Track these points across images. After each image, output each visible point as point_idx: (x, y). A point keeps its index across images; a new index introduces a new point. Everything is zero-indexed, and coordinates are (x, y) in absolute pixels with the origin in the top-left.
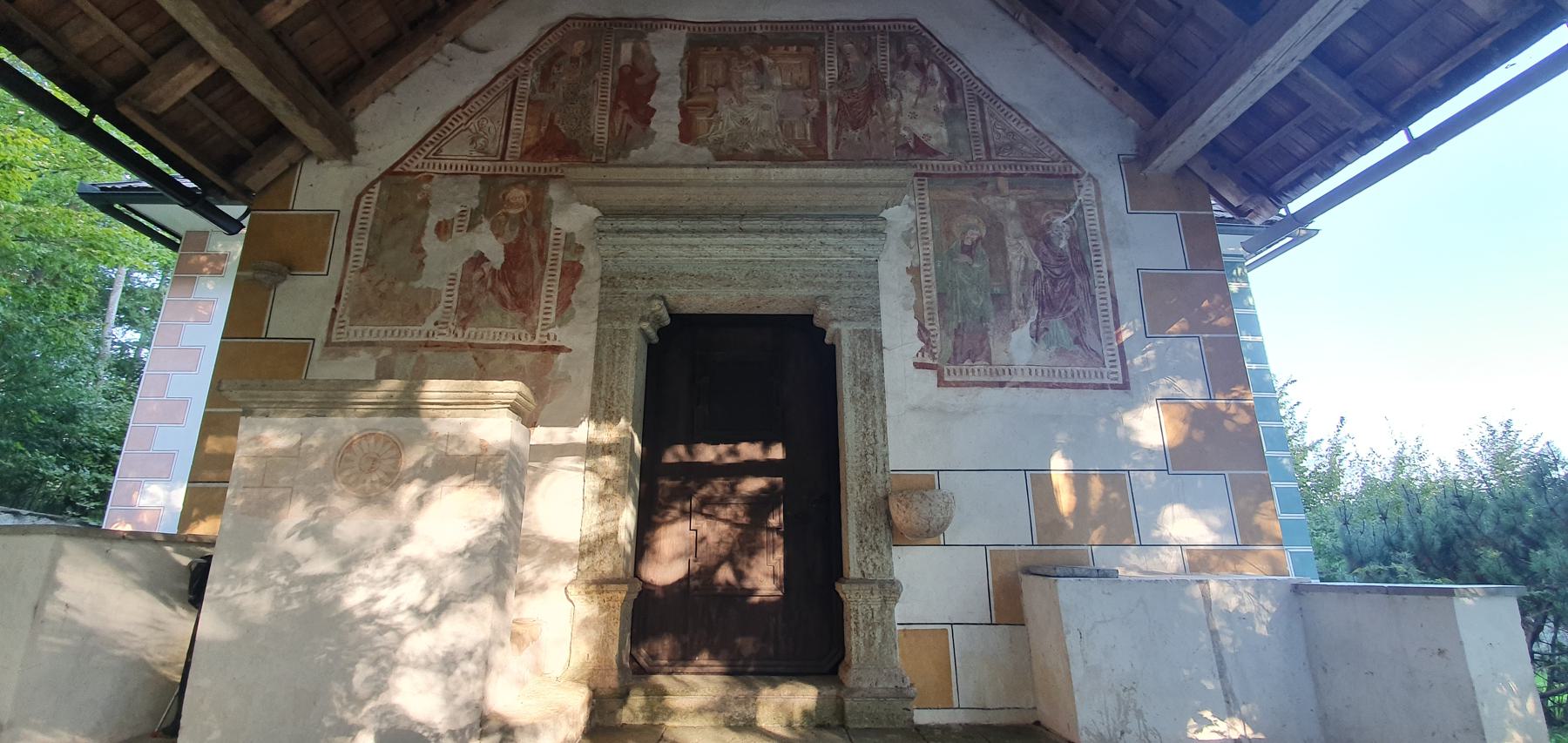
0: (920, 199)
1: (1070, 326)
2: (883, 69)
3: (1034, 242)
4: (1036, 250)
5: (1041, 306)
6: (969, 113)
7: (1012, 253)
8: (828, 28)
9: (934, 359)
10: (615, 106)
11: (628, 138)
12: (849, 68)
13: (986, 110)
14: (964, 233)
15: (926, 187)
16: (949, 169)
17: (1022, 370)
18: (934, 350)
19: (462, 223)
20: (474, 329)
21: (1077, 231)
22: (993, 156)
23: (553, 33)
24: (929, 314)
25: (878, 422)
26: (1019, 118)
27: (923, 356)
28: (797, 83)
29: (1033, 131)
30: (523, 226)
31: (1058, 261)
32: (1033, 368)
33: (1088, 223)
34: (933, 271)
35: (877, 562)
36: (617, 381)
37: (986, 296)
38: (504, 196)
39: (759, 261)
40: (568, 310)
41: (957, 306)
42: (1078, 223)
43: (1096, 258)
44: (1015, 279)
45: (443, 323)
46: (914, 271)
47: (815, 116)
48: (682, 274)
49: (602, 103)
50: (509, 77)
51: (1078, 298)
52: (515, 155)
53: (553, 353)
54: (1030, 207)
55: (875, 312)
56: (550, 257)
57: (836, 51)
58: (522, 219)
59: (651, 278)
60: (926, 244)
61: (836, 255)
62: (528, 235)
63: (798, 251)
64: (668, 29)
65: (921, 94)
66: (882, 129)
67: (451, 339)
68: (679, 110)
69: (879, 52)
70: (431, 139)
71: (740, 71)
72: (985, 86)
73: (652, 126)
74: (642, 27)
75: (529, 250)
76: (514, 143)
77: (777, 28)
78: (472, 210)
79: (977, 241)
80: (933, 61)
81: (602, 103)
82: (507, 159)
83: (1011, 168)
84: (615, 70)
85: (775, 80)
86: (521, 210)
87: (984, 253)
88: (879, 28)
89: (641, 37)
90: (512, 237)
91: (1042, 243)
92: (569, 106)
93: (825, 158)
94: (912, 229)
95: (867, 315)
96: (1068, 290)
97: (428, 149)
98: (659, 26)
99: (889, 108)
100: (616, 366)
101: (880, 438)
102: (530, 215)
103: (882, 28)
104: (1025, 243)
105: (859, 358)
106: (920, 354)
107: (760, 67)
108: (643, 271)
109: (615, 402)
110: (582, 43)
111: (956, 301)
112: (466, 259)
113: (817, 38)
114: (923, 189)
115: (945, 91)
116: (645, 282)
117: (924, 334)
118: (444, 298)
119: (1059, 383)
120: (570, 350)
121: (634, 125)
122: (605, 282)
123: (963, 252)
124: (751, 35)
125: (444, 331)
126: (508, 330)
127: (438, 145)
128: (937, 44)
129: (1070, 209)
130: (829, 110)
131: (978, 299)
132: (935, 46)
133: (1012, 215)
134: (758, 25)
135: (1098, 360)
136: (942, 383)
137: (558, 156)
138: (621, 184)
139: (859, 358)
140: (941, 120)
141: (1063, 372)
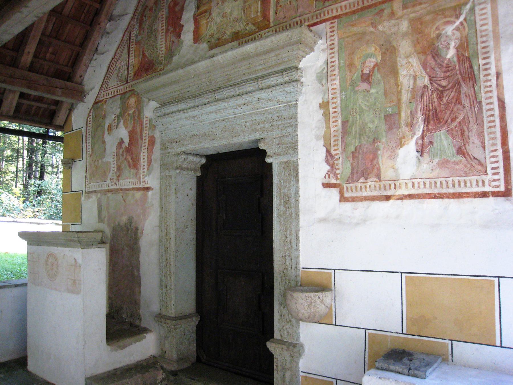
1: (454, 138)
3: (423, 58)
4: (425, 66)
5: (427, 121)
7: (403, 73)
9: (337, 179)
14: (364, 63)
15: (335, 29)
17: (406, 183)
18: (338, 172)
21: (467, 37)
25: (293, 232)
27: (329, 177)
30: (134, 120)
31: (445, 72)
32: (416, 182)
33: (479, 23)
35: (289, 330)
39: (228, 119)
41: (356, 131)
42: (468, 26)
43: (484, 61)
44: (405, 97)
46: (324, 106)
48: (193, 136)
51: (464, 107)
53: (147, 191)
54: (421, 23)
61: (269, 106)
63: (245, 108)
79: (374, 68)
90: (130, 129)
91: (430, 57)
94: (324, 69)
96: (454, 101)
101: (294, 244)
102: (137, 113)
104: (415, 62)
105: (282, 184)
106: (327, 176)
111: (356, 127)
117: (330, 159)
119: (440, 194)
122: (162, 147)
129: (460, 14)
131: (373, 122)
135: (480, 168)
136: (343, 199)
138: (164, 86)
139: (282, 184)
141: (444, 183)
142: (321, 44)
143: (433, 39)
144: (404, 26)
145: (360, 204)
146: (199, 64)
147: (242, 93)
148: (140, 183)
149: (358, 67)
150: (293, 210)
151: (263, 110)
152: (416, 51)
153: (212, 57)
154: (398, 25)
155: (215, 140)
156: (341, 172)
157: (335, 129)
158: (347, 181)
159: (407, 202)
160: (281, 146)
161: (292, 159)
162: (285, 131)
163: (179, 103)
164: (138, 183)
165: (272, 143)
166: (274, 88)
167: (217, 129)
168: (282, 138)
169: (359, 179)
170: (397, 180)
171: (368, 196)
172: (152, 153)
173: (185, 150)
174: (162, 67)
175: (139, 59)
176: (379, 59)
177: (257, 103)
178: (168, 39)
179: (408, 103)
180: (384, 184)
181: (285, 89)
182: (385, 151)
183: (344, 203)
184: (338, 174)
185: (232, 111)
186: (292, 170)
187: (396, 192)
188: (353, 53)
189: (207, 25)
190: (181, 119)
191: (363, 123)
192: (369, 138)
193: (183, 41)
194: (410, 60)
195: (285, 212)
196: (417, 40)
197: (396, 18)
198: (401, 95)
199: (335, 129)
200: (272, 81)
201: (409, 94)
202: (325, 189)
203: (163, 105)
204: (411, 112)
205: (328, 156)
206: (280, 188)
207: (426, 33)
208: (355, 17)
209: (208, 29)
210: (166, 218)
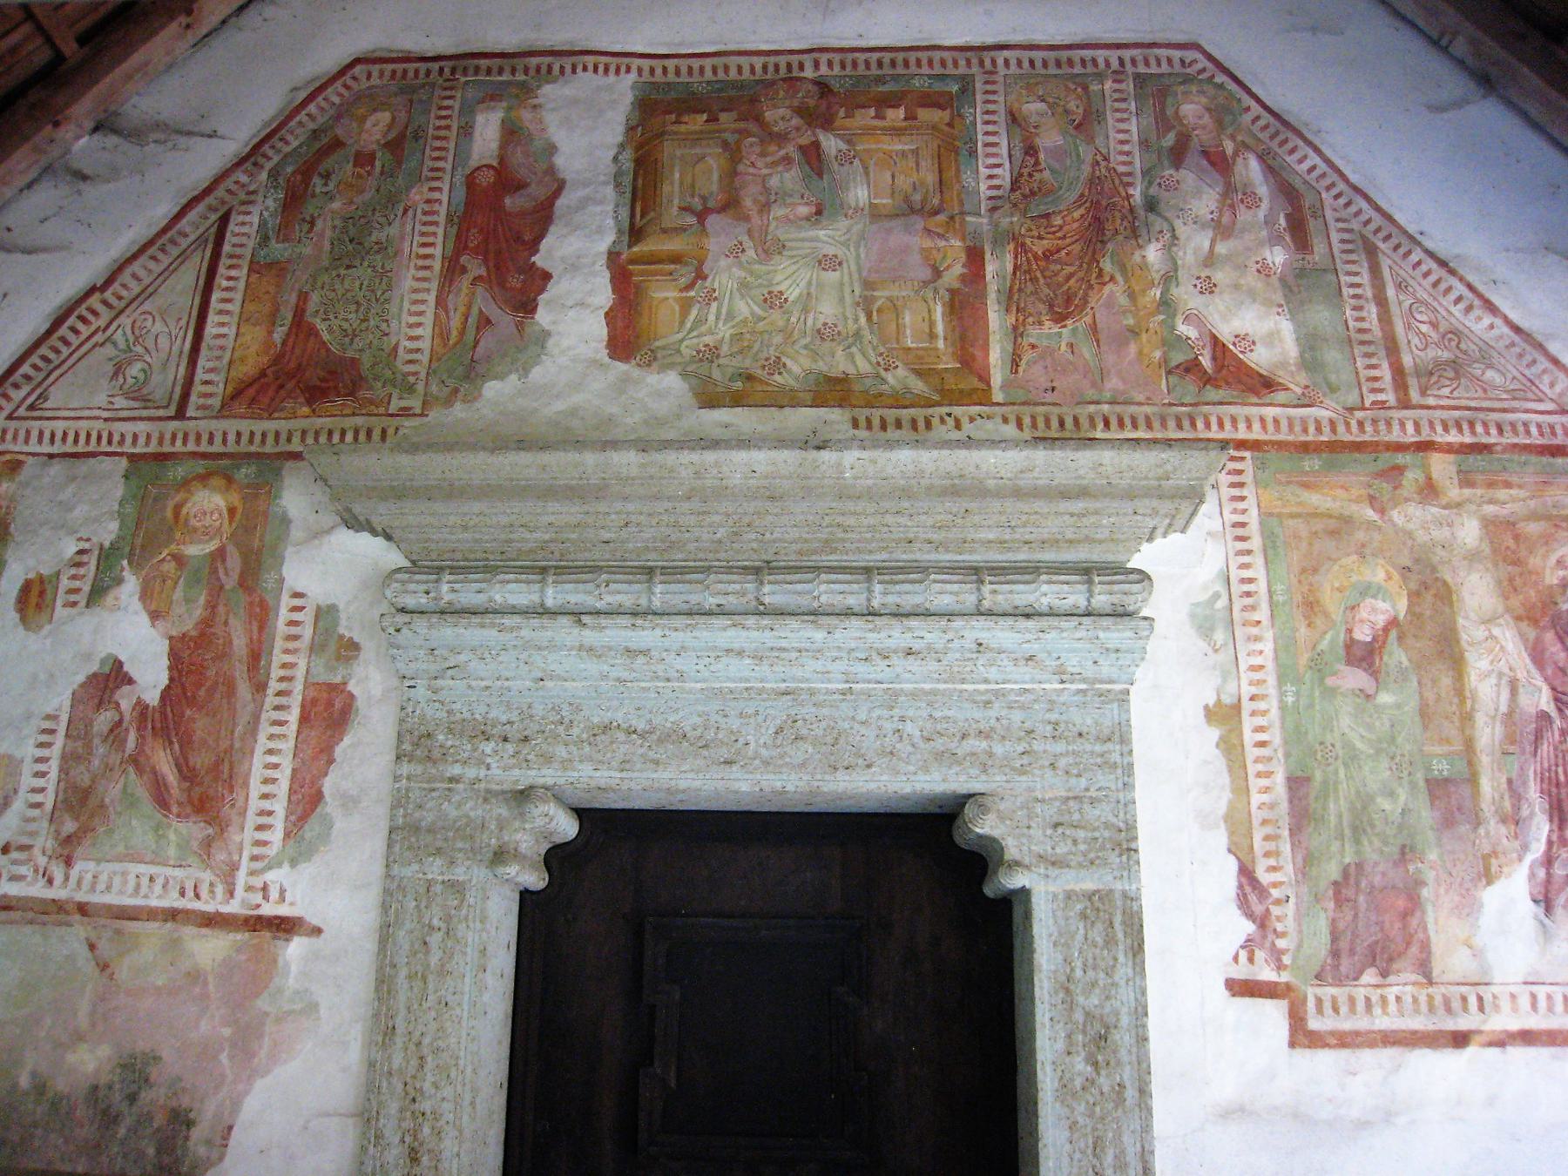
0: (1235, 511)
2: (1124, 163)
3: (1532, 634)
6: (1344, 279)
7: (1478, 664)
8: (981, 63)
9: (1280, 967)
10: (452, 269)
11: (480, 350)
12: (1037, 163)
13: (1386, 273)
15: (1248, 478)
16: (1305, 431)
17: (1513, 996)
19: (77, 584)
20: (91, 865)
22: (1414, 395)
23: (320, 99)
24: (1267, 838)
26: (1470, 295)
28: (907, 199)
29: (1506, 330)
30: (217, 590)
32: (1541, 992)
34: (1274, 713)
36: (433, 1026)
37: (1413, 786)
38: (178, 508)
39: (812, 692)
40: (314, 820)
41: (1340, 816)
44: (1487, 734)
45: (22, 848)
46: (1224, 715)
47: (956, 285)
48: (606, 728)
49: (421, 263)
50: (211, 209)
52: (210, 401)
53: (275, 938)
54: (1516, 537)
55: (1124, 843)
56: (276, 673)
57: (1001, 117)
58: (214, 571)
59: (526, 739)
60: (1257, 639)
61: (1020, 678)
62: (227, 614)
63: (913, 664)
64: (590, 73)
65: (1222, 230)
66: (1130, 321)
67: (38, 890)
68: (607, 275)
69: (1110, 122)
70: (26, 368)
71: (765, 171)
72: (1378, 209)
73: (543, 316)
74: (526, 71)
75: (224, 655)
76: (212, 370)
77: (855, 64)
78: (101, 547)
79: (1386, 630)
80: (1247, 147)
81: (421, 263)
82: (190, 412)
83: (1460, 430)
84: (459, 179)
85: (851, 195)
86: (212, 546)
87: (1406, 663)
88: (1108, 64)
89: (525, 92)
90: (187, 618)
92: (343, 272)
93: (982, 396)
94: (1217, 596)
95: (1103, 848)
97: (17, 395)
98: (568, 69)
99: (1144, 266)
100: (431, 986)
102: (234, 561)
103: (1115, 65)
104: (1510, 642)
105: (1079, 973)
106: (1243, 955)
107: (813, 157)
108: (504, 718)
109: (427, 1086)
110: (384, 117)
111: (1337, 800)
112: (81, 678)
113: (955, 88)
114: (1241, 485)
115: (1282, 221)
116: (510, 748)
117: (1253, 898)
118: (27, 781)
120: (317, 931)
121: (493, 311)
122: (407, 747)
123: (1352, 660)
124: (791, 81)
125: (23, 870)
126: (169, 871)
127: (40, 383)
128: (1253, 103)
130: (990, 268)
131: (1392, 794)
132: (1248, 109)
133: (1472, 557)
134: (808, 60)
136: (1301, 1036)
137: (309, 403)
140: (1279, 297)
142: (1209, 517)
143: (1551, 587)
144: (1469, 532)
145: (1367, 1056)
146: (741, 456)
147: (894, 609)
148: (231, 894)
149: (1334, 617)
150: (1127, 1075)
151: (983, 687)
152: (1508, 610)
153: (819, 448)
154: (1450, 525)
155: (735, 768)
156: (1292, 946)
157: (1265, 798)
158: (1318, 977)
159: (1517, 1053)
160: (1068, 832)
161: (1118, 886)
162: (1083, 782)
163: (550, 579)
164: (212, 892)
165: (1029, 817)
166: (1054, 621)
167: (752, 720)
168: (1071, 803)
169: (1361, 972)
170: (1486, 984)
171: (1393, 1031)
172: (331, 761)
173: (562, 781)
174: (415, 403)
175: (270, 333)
176: (1402, 605)
177: (969, 659)
178: (458, 301)
179: (1498, 754)
180: (1444, 995)
181: (1101, 635)
182: (1442, 891)
183: (1307, 1050)
184: (1283, 952)
185: (840, 666)
186: (1117, 926)
187: (1484, 1022)
188: (1315, 570)
189: (685, 312)
190: (552, 647)
191: (1358, 792)
192: (1385, 843)
193: (546, 334)
194: (1496, 631)
195: (1093, 1083)
196: (1511, 580)
197: (1444, 502)
198: (1473, 727)
199: (1265, 798)
200: (1046, 594)
201: (1499, 730)
202: (1238, 1000)
203: (425, 565)
204: (1510, 781)
205: (1248, 889)
206: (1067, 991)
207: (1530, 567)
208: (1311, 463)
209: (688, 325)
210: (414, 1077)
